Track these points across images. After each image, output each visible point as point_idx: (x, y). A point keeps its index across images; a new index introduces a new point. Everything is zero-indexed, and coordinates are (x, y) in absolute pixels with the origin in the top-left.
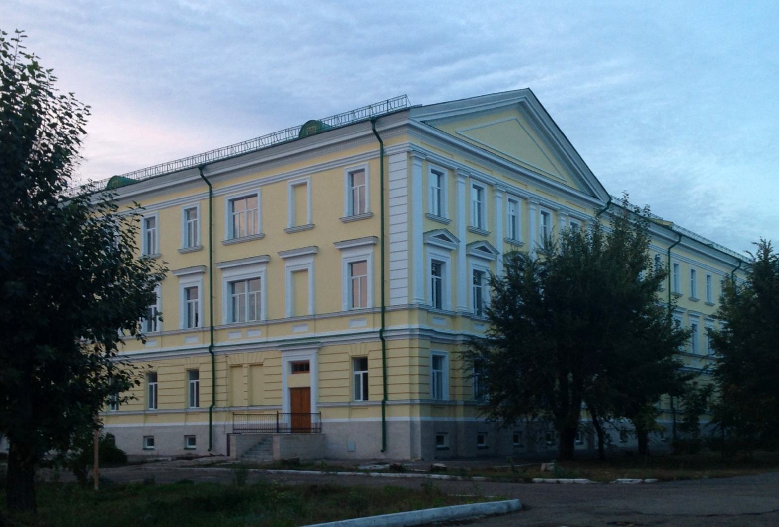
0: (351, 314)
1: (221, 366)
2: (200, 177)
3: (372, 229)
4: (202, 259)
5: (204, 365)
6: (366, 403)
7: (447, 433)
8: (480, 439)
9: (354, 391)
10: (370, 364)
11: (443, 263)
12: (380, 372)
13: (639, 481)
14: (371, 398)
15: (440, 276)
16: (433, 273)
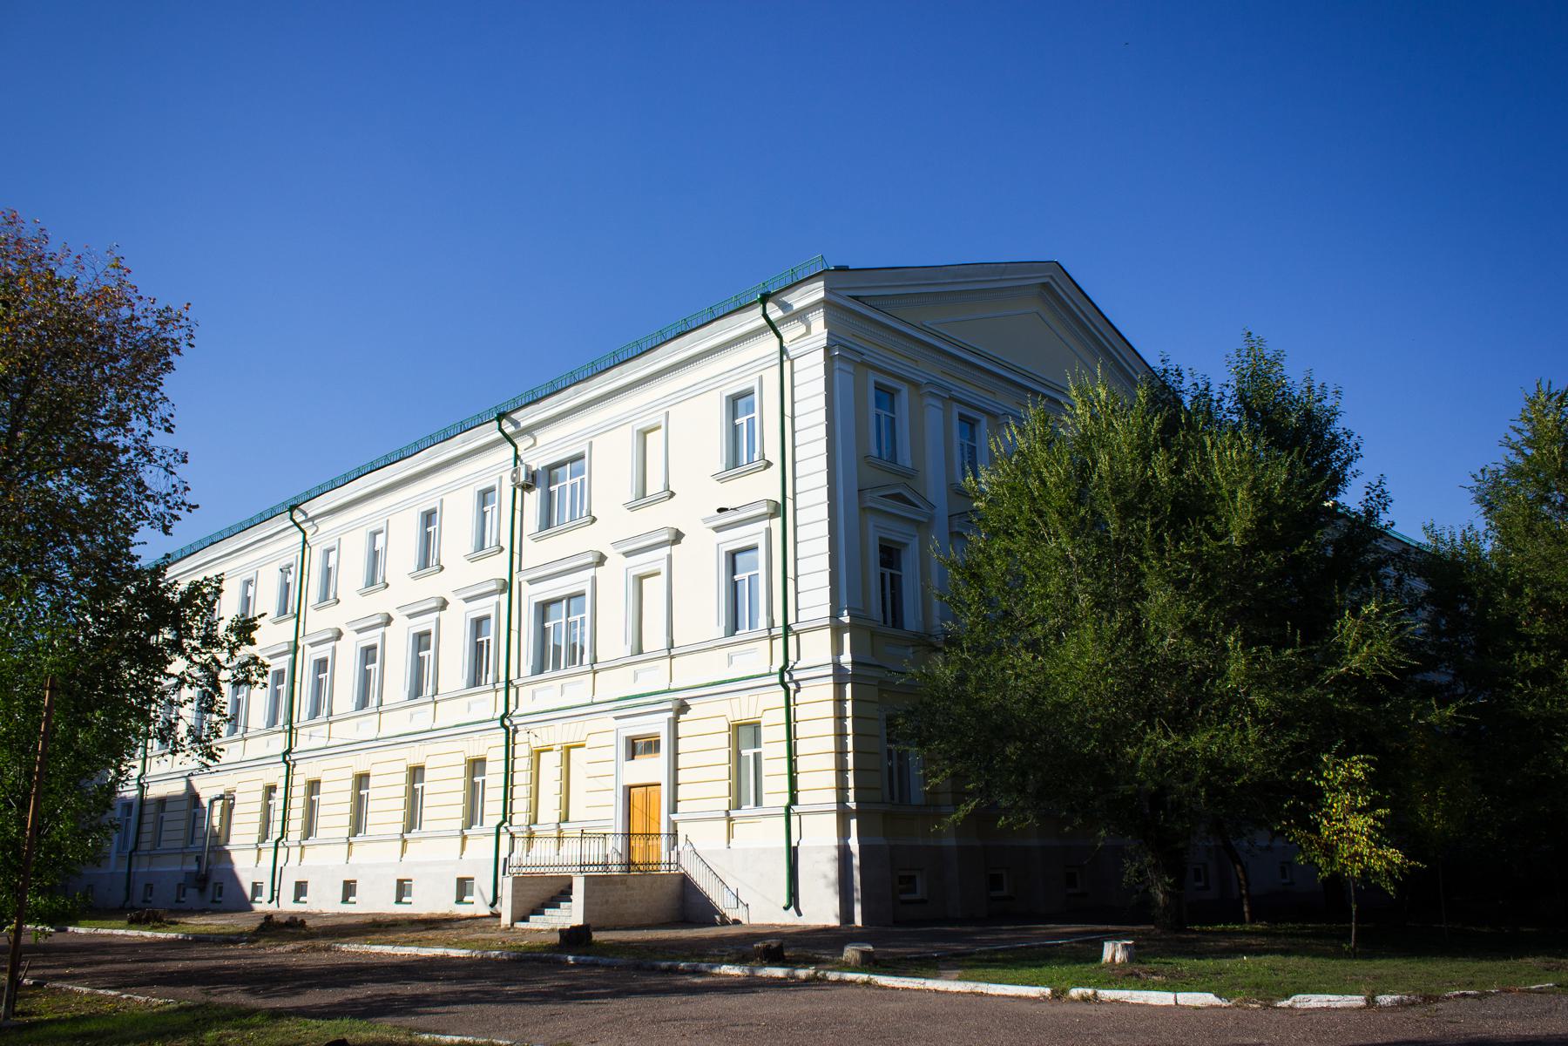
0: (770, 674)
1: (521, 751)
2: (499, 435)
3: (766, 486)
4: (497, 567)
5: (491, 746)
6: (759, 811)
7: (799, 914)
8: (995, 882)
9: (1486, 964)
10: (766, 734)
11: (905, 545)
12: (783, 749)
13: (1358, 1001)
14: (767, 800)
15: (899, 569)
16: (883, 563)
